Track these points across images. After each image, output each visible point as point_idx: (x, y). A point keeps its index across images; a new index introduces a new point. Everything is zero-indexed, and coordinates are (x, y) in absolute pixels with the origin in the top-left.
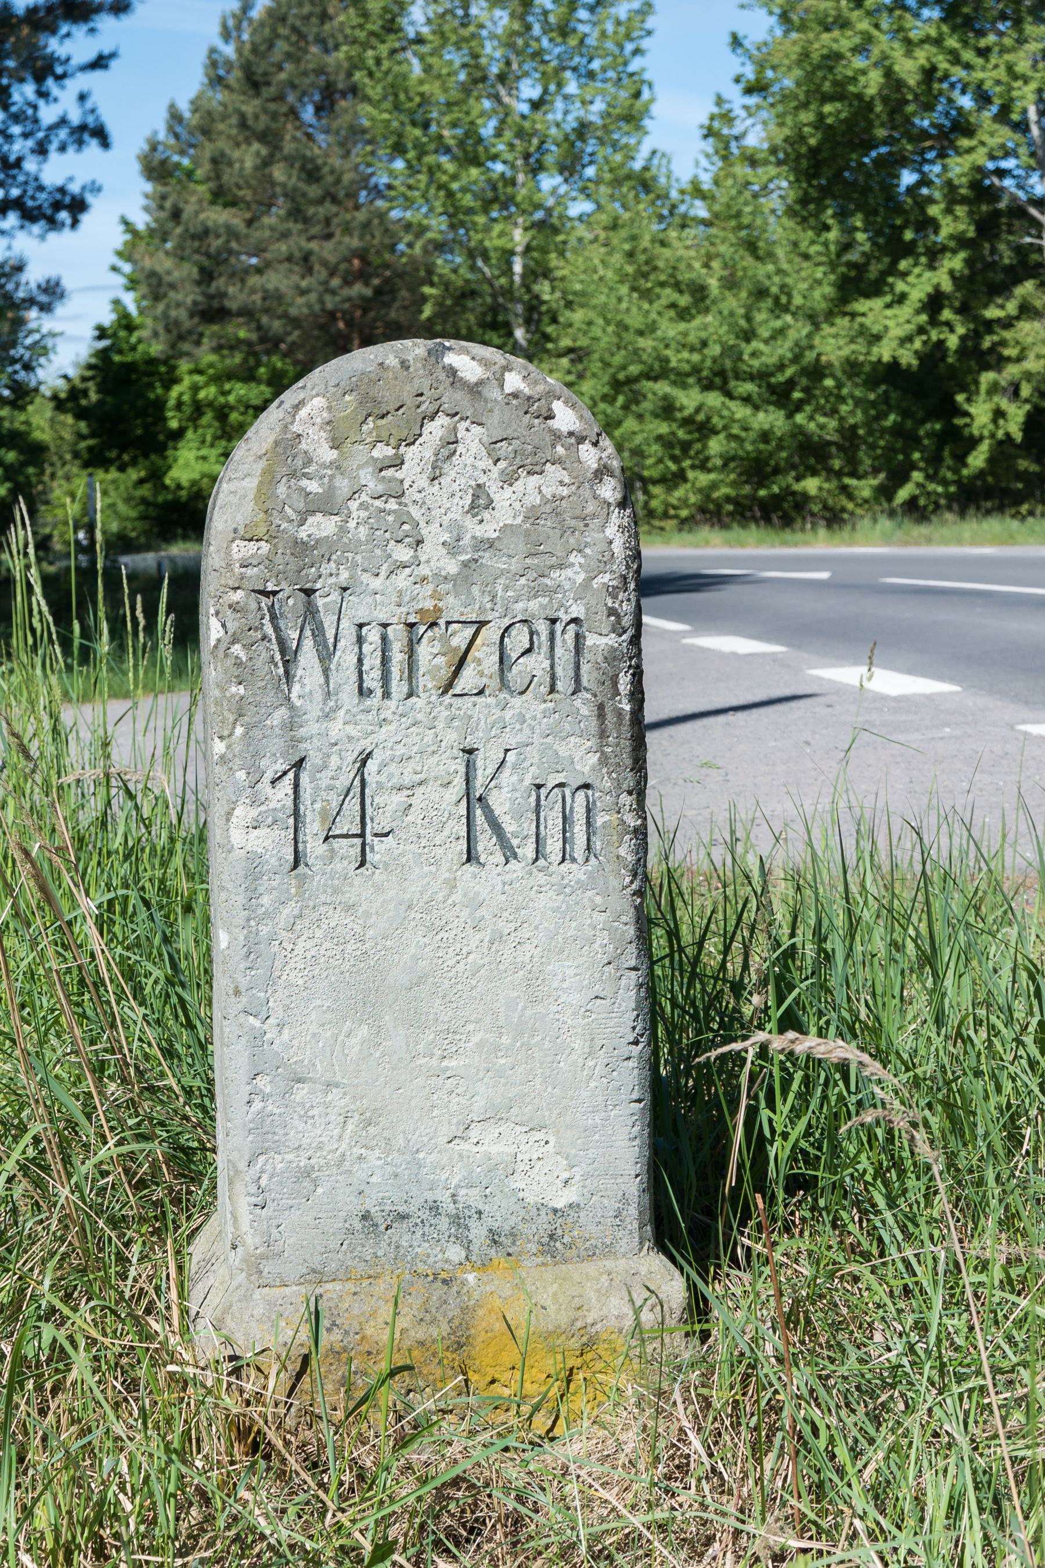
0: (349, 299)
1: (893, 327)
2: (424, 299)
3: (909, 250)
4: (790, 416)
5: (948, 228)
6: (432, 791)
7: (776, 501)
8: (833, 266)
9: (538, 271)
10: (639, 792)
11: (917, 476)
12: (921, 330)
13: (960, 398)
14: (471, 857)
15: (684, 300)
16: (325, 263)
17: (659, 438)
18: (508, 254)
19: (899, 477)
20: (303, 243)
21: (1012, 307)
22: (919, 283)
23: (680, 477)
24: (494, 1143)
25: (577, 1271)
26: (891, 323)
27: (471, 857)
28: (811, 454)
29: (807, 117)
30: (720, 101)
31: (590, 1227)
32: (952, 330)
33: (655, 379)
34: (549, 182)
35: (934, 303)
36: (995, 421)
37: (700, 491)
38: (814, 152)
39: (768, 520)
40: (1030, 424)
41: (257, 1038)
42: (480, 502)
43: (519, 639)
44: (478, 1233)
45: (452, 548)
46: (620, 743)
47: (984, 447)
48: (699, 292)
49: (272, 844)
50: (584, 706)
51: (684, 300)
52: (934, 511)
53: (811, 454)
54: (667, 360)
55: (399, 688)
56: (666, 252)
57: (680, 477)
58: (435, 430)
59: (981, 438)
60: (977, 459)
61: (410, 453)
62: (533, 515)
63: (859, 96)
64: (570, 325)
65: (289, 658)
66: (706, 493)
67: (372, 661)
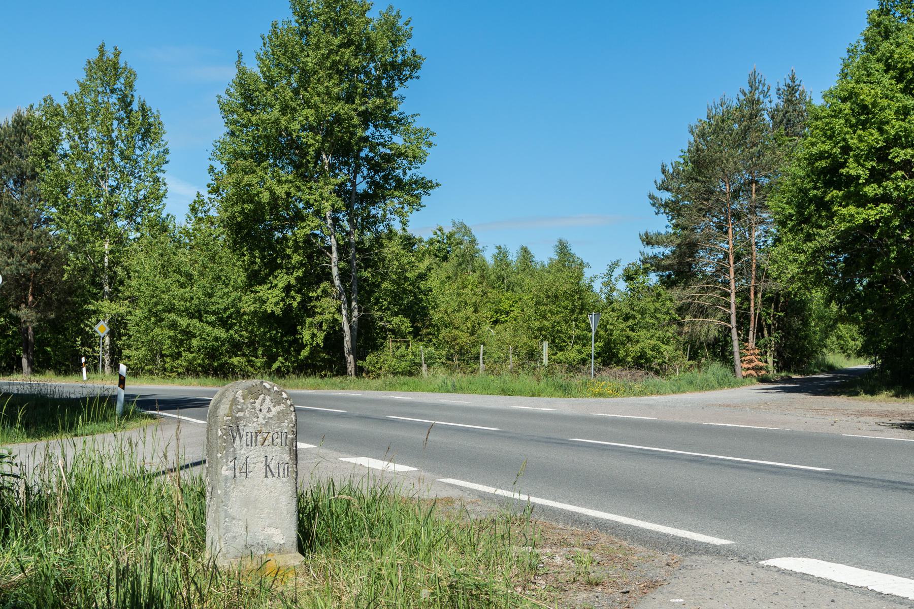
0: (30, 269)
1: (272, 297)
2: (64, 271)
3: (280, 266)
4: (227, 331)
5: (296, 258)
6: (259, 464)
7: (222, 366)
8: (246, 270)
9: (114, 263)
10: (296, 464)
11: (280, 358)
12: (283, 300)
13: (299, 328)
14: (266, 476)
15: (182, 280)
16: (19, 252)
17: (170, 337)
18: (103, 255)
19: (272, 358)
20: (10, 243)
21: (319, 292)
22: (282, 279)
23: (179, 355)
24: (269, 531)
25: (284, 556)
26: (270, 296)
27: (266, 476)
28: (236, 347)
29: (237, 208)
30: (198, 195)
31: (287, 547)
32: (295, 300)
33: (170, 312)
34: (121, 223)
35: (288, 288)
36: (312, 338)
37: (188, 361)
38: (239, 224)
39: (217, 375)
40: (326, 339)
41: (226, 510)
42: (269, 410)
43: (276, 435)
44: (266, 548)
45: (264, 419)
46: (293, 455)
47: (308, 348)
48: (189, 276)
49: (229, 473)
50: (287, 448)
51: (182, 280)
52: (287, 374)
53: (236, 347)
54: (174, 305)
55: (254, 444)
56: (176, 258)
57: (179, 355)
58: (261, 397)
59: (307, 345)
60: (305, 353)
61: (257, 401)
62: (278, 413)
63: (259, 203)
64: (130, 287)
65: (234, 438)
66: (190, 362)
67: (249, 439)
